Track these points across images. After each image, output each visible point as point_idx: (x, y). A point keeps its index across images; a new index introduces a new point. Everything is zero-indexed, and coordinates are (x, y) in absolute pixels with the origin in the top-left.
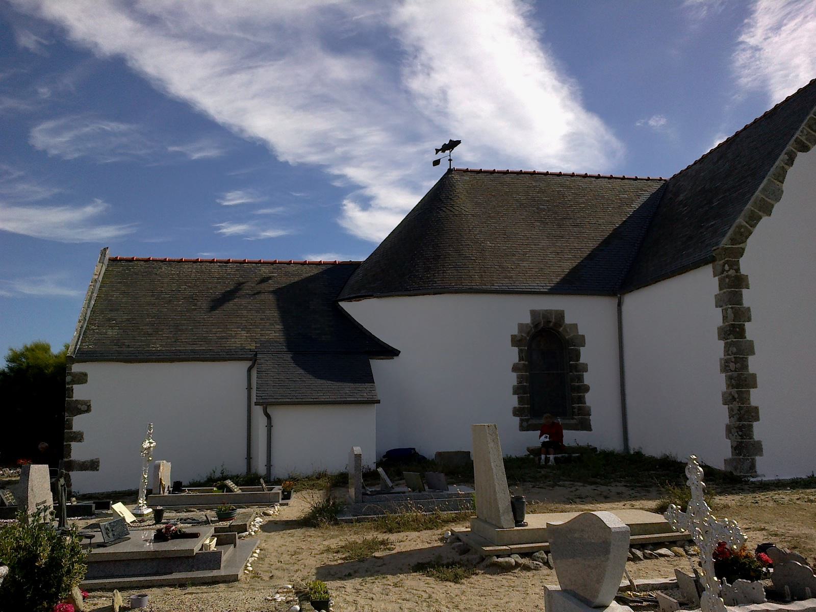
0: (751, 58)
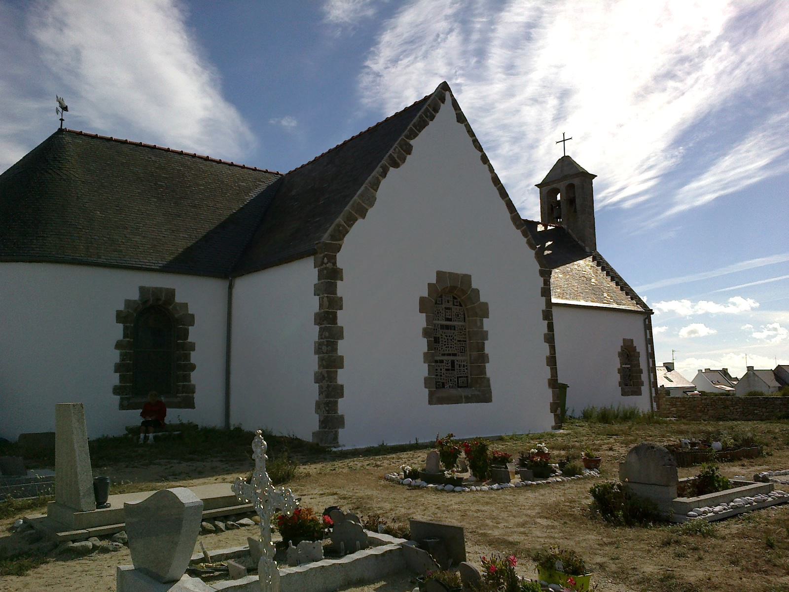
0: (373, 82)
